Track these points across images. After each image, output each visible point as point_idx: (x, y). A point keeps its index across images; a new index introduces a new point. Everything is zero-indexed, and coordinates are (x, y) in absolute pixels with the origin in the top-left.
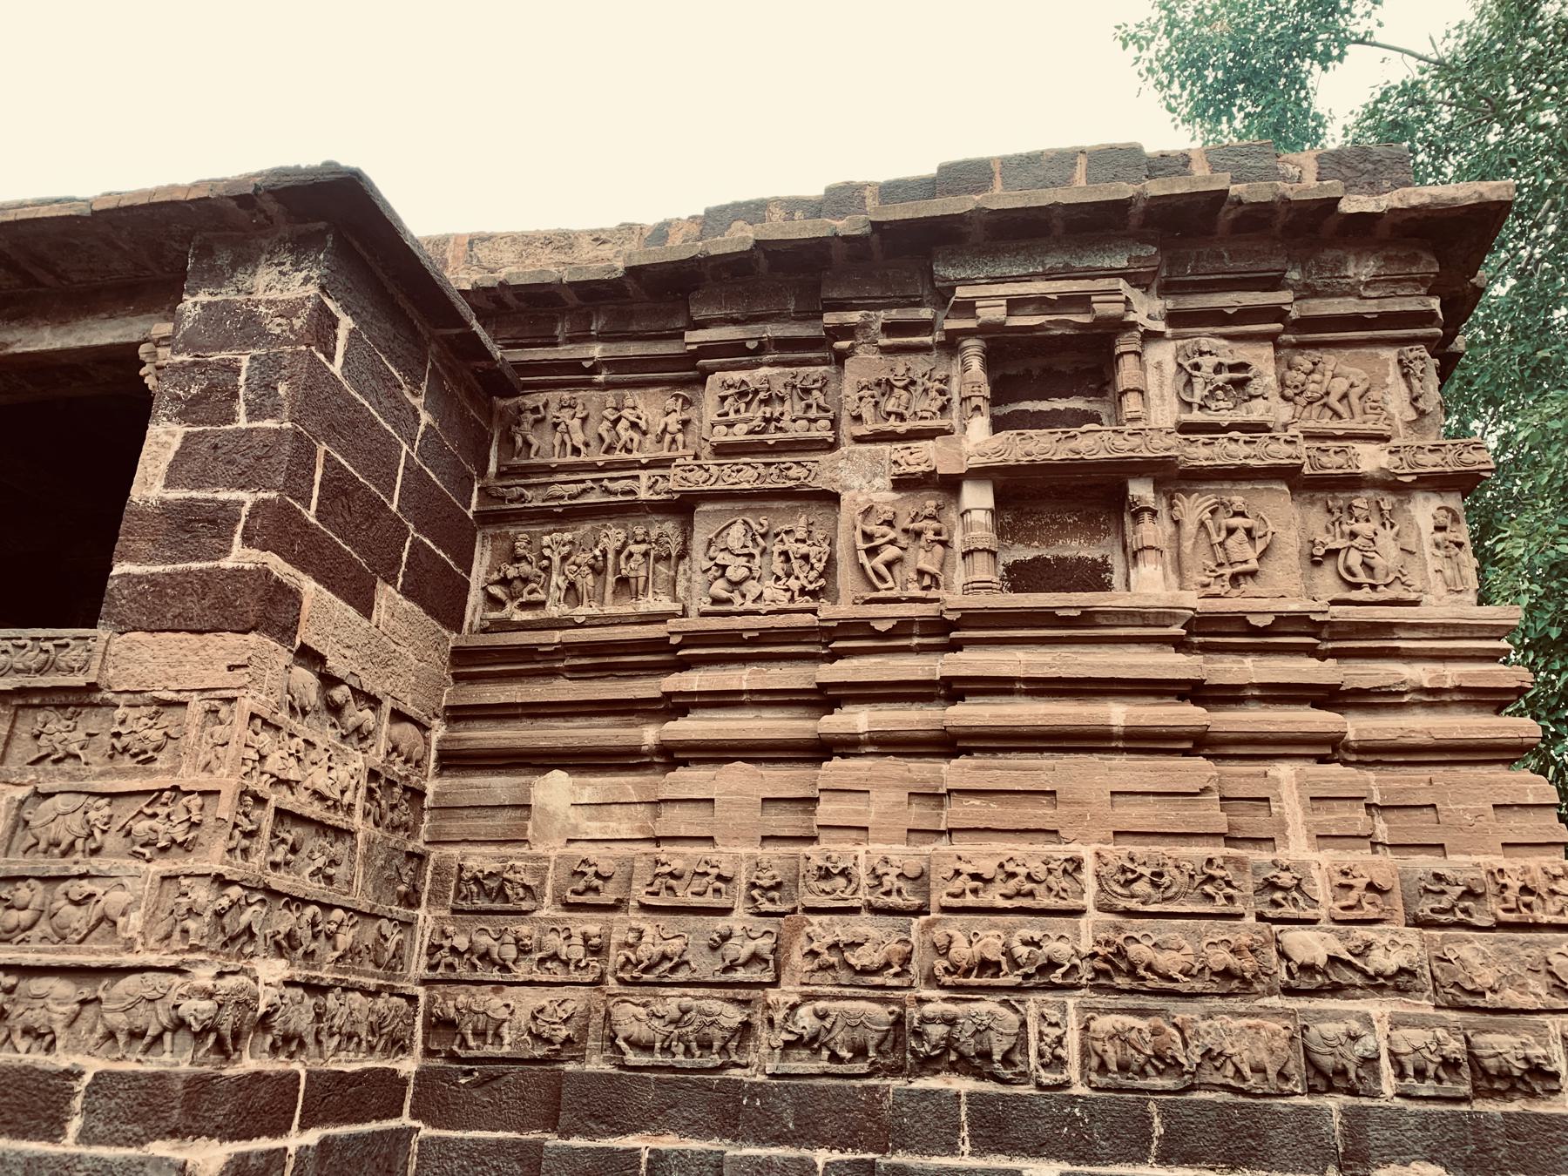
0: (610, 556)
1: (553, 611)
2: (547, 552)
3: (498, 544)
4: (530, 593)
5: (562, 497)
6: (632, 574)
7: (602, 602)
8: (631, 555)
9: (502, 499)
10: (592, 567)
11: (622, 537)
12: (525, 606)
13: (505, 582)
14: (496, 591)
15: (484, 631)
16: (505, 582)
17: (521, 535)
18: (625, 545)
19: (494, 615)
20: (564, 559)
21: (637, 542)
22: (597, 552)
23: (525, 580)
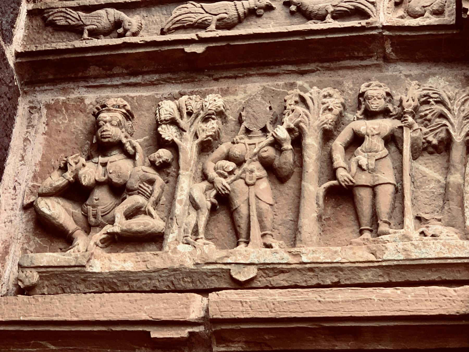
0: (312, 142)
1: (180, 253)
2: (168, 133)
3: (62, 120)
4: (130, 215)
5: (203, 26)
6: (364, 179)
7: (294, 237)
8: (357, 140)
9: (77, 30)
10: (268, 165)
11: (335, 102)
12: (116, 242)
13: (75, 192)
14: (59, 211)
15: (26, 290)
16: (75, 192)
17: (114, 101)
18: (339, 122)
19: (52, 258)
20: (205, 147)
21: (369, 115)
22: (282, 132)
23: (119, 190)
